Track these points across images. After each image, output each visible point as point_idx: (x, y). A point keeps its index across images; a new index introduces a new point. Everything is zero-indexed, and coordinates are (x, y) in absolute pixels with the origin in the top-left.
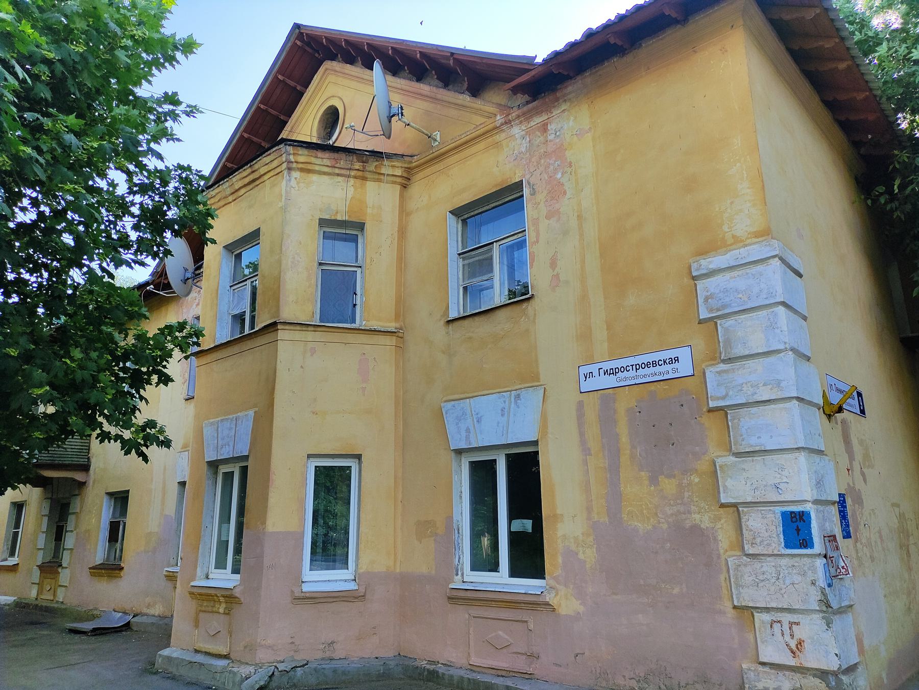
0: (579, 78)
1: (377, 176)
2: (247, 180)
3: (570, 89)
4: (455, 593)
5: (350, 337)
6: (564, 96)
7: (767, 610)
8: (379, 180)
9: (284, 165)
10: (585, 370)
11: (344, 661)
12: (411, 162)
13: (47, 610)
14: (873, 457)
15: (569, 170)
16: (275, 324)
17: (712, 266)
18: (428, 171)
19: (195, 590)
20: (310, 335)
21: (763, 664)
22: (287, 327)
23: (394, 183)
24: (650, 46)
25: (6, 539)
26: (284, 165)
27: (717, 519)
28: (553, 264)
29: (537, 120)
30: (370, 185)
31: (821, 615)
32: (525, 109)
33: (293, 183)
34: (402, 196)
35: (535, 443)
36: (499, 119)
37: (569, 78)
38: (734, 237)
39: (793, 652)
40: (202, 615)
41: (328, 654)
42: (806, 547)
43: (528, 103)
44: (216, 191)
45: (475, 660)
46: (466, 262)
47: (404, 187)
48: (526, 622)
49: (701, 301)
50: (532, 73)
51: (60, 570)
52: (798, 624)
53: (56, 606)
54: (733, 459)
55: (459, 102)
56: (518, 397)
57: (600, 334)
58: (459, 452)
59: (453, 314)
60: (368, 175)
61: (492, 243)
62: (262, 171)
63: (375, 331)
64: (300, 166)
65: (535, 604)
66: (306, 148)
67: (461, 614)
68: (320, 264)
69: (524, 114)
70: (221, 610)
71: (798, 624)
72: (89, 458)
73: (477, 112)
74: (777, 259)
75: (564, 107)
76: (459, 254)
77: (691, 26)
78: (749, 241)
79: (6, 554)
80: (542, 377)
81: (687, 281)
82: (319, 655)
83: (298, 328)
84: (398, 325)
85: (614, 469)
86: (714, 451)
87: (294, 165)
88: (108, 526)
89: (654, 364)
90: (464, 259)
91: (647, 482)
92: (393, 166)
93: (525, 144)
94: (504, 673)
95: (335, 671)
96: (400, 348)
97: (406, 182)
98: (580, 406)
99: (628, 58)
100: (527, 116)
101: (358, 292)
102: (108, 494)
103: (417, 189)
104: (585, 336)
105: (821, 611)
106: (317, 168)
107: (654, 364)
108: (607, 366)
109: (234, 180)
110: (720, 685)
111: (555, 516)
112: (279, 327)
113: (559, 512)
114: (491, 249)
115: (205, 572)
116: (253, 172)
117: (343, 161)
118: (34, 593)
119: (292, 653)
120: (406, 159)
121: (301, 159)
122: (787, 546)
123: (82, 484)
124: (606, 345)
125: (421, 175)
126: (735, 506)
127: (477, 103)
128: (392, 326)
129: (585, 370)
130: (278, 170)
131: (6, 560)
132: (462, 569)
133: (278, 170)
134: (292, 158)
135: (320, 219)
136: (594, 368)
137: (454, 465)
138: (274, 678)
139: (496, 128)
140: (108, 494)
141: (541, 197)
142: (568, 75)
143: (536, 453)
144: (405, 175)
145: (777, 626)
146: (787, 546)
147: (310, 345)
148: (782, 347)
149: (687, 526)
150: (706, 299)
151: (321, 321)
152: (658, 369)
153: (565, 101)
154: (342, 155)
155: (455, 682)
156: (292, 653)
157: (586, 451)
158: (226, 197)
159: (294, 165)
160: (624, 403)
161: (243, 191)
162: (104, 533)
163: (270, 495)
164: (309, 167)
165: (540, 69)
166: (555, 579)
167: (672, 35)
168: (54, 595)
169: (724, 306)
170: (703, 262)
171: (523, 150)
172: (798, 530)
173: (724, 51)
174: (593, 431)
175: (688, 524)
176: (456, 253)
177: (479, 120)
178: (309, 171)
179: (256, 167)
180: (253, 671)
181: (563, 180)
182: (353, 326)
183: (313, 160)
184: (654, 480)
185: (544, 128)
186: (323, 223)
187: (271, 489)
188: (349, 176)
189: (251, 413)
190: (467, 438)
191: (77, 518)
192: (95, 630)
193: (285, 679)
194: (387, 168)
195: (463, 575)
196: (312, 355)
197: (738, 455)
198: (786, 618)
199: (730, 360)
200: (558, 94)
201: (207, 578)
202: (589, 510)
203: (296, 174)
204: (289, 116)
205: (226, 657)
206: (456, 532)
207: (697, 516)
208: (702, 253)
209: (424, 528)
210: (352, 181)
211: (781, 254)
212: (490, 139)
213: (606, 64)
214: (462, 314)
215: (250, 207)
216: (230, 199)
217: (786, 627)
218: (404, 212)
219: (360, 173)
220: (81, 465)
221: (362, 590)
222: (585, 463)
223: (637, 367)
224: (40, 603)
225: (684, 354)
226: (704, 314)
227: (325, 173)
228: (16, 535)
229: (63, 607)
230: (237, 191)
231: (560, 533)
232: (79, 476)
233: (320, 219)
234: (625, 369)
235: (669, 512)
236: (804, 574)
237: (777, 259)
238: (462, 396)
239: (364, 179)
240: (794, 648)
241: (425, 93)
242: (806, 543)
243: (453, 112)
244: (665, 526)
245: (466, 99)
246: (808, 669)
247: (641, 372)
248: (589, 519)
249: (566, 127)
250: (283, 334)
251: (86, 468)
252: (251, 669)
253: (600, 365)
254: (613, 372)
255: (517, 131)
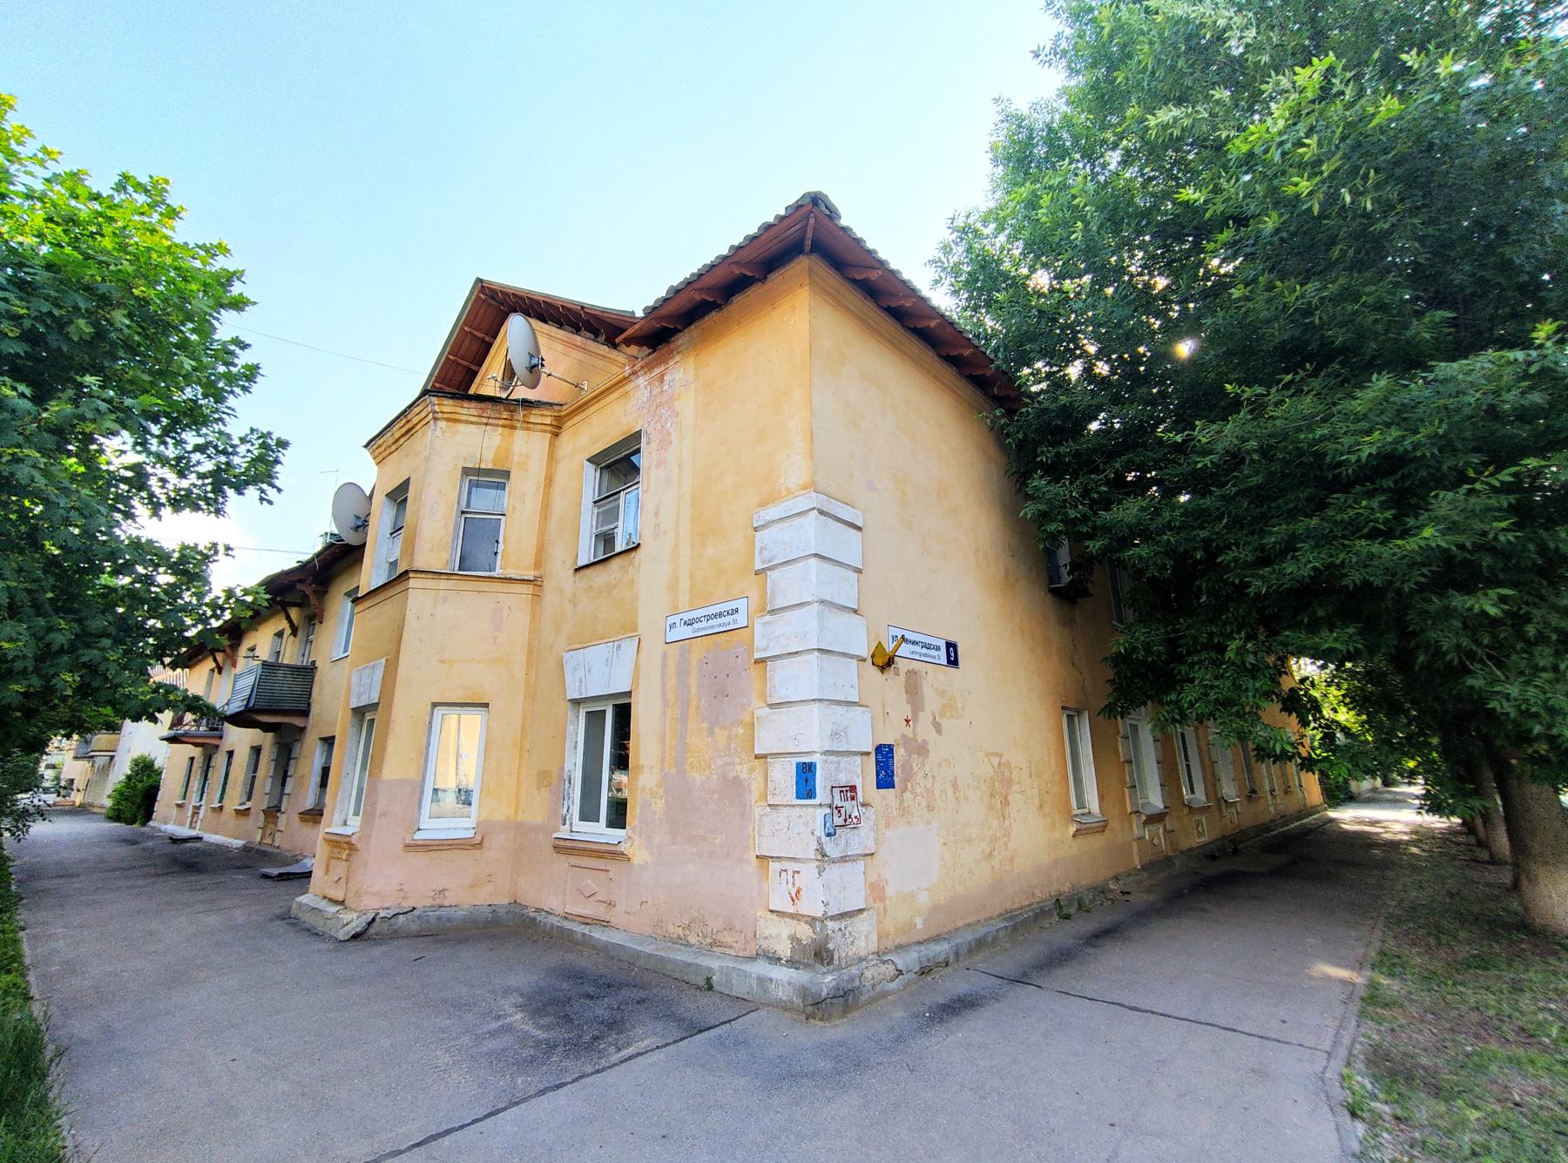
0: (686, 331)
1: (525, 425)
2: (404, 430)
3: (680, 342)
4: (562, 843)
5: (484, 586)
6: (677, 348)
7: (779, 858)
8: (528, 429)
9: (431, 416)
10: (671, 620)
11: (454, 909)
12: (561, 411)
13: (264, 854)
14: (963, 708)
15: (676, 420)
16: (406, 572)
17: (768, 518)
18: (575, 420)
19: (328, 837)
20: (443, 583)
21: (772, 911)
22: (418, 575)
23: (545, 431)
24: (738, 300)
25: (245, 784)
26: (431, 416)
27: (753, 769)
28: (657, 514)
29: (657, 371)
30: (519, 435)
31: (817, 863)
32: (646, 360)
33: (439, 432)
34: (552, 444)
35: (629, 694)
36: (628, 371)
37: (675, 332)
38: (787, 488)
39: (793, 900)
40: (334, 862)
41: (438, 901)
42: (810, 798)
43: (649, 354)
44: (382, 440)
45: (570, 909)
46: (601, 510)
47: (557, 435)
48: (608, 871)
49: (757, 552)
50: (637, 326)
51: (279, 814)
52: (798, 872)
53: (271, 850)
54: (767, 710)
55: (601, 353)
56: (619, 647)
57: (684, 584)
58: (577, 703)
59: (582, 562)
60: (515, 423)
61: (619, 492)
62: (415, 421)
63: (510, 579)
64: (446, 416)
65: (613, 854)
66: (451, 398)
67: (563, 862)
68: (463, 512)
69: (647, 365)
70: (344, 857)
71: (798, 872)
72: (309, 705)
73: (614, 362)
74: (815, 511)
75: (678, 358)
76: (595, 502)
77: (769, 285)
78: (796, 494)
79: (244, 798)
80: (639, 627)
81: (750, 531)
82: (429, 902)
83: (431, 576)
84: (537, 574)
85: (684, 719)
86: (756, 702)
87: (440, 415)
88: (320, 771)
89: (720, 615)
90: (599, 507)
91: (706, 734)
92: (542, 415)
93: (647, 394)
94: (589, 921)
95: (439, 918)
96: (536, 597)
97: (556, 431)
98: (665, 655)
99: (725, 312)
100: (649, 367)
101: (501, 540)
102: (320, 739)
103: (566, 436)
104: (673, 586)
105: (817, 860)
106: (463, 418)
107: (720, 615)
108: (686, 617)
109: (394, 429)
110: (741, 932)
111: (638, 766)
112: (411, 575)
113: (641, 763)
114: (619, 498)
115: (343, 819)
116: (408, 422)
117: (490, 410)
118: (258, 839)
119: (400, 900)
120: (556, 407)
121: (446, 409)
122: (798, 797)
123: (303, 729)
124: (688, 595)
125: (569, 424)
126: (764, 757)
127: (614, 354)
128: (530, 575)
129: (671, 620)
130: (426, 420)
131: (244, 804)
132: (571, 819)
133: (426, 420)
134: (437, 408)
135: (463, 468)
136: (676, 619)
137: (570, 715)
138: (374, 925)
139: (625, 378)
140: (320, 739)
141: (654, 446)
142: (675, 328)
143: (630, 704)
144: (555, 423)
145: (783, 874)
146: (798, 797)
147: (442, 593)
148: (809, 599)
149: (731, 777)
150: (762, 550)
151: (460, 570)
152: (723, 620)
153: (678, 353)
154: (490, 405)
155: (547, 929)
156: (400, 900)
157: (665, 703)
158: (389, 447)
159: (440, 415)
160: (698, 651)
161: (402, 440)
162: (316, 779)
163: (389, 742)
164: (456, 417)
165: (642, 322)
166: (633, 829)
167: (754, 292)
168: (273, 840)
169: (773, 558)
170: (762, 513)
171: (645, 400)
172: (807, 780)
173: (794, 308)
174: (672, 682)
175: (732, 775)
176: (591, 501)
177: (616, 369)
178: (455, 421)
179: (410, 417)
180: (355, 917)
181: (671, 430)
182: (492, 574)
183: (459, 410)
184: (711, 733)
185: (661, 378)
186: (466, 471)
187: (390, 736)
188: (498, 425)
189: (383, 661)
190: (580, 690)
191: (297, 763)
192: (280, 875)
193: (385, 926)
194: (535, 417)
195: (571, 824)
196: (443, 603)
197: (771, 706)
198: (791, 866)
199: (773, 612)
200: (672, 346)
201: (345, 824)
202: (662, 761)
203: (442, 424)
204: (480, 365)
205: (342, 903)
206: (567, 782)
207: (738, 767)
208: (763, 504)
209: (544, 778)
210: (500, 430)
211: (819, 507)
212: (622, 390)
213: (707, 318)
214: (592, 560)
215: (407, 456)
216: (393, 448)
217: (790, 874)
218: (552, 458)
219: (508, 422)
220: (300, 711)
221: (478, 838)
222: (664, 714)
223: (709, 617)
224: (263, 848)
225: (741, 604)
226: (758, 566)
227: (472, 423)
228: (254, 777)
229: (276, 851)
230: (398, 440)
231: (640, 784)
232: (298, 722)
233: (463, 468)
234: (699, 620)
235: (720, 763)
236: (807, 824)
237: (815, 511)
238: (581, 646)
239: (513, 428)
240: (794, 896)
241: (578, 344)
242: (810, 794)
243: (598, 362)
244: (715, 777)
245: (604, 349)
246: (803, 916)
247: (711, 622)
248: (662, 770)
249: (677, 378)
250: (413, 582)
251: (305, 713)
252: (354, 915)
253: (681, 616)
254: (689, 623)
255: (642, 381)
